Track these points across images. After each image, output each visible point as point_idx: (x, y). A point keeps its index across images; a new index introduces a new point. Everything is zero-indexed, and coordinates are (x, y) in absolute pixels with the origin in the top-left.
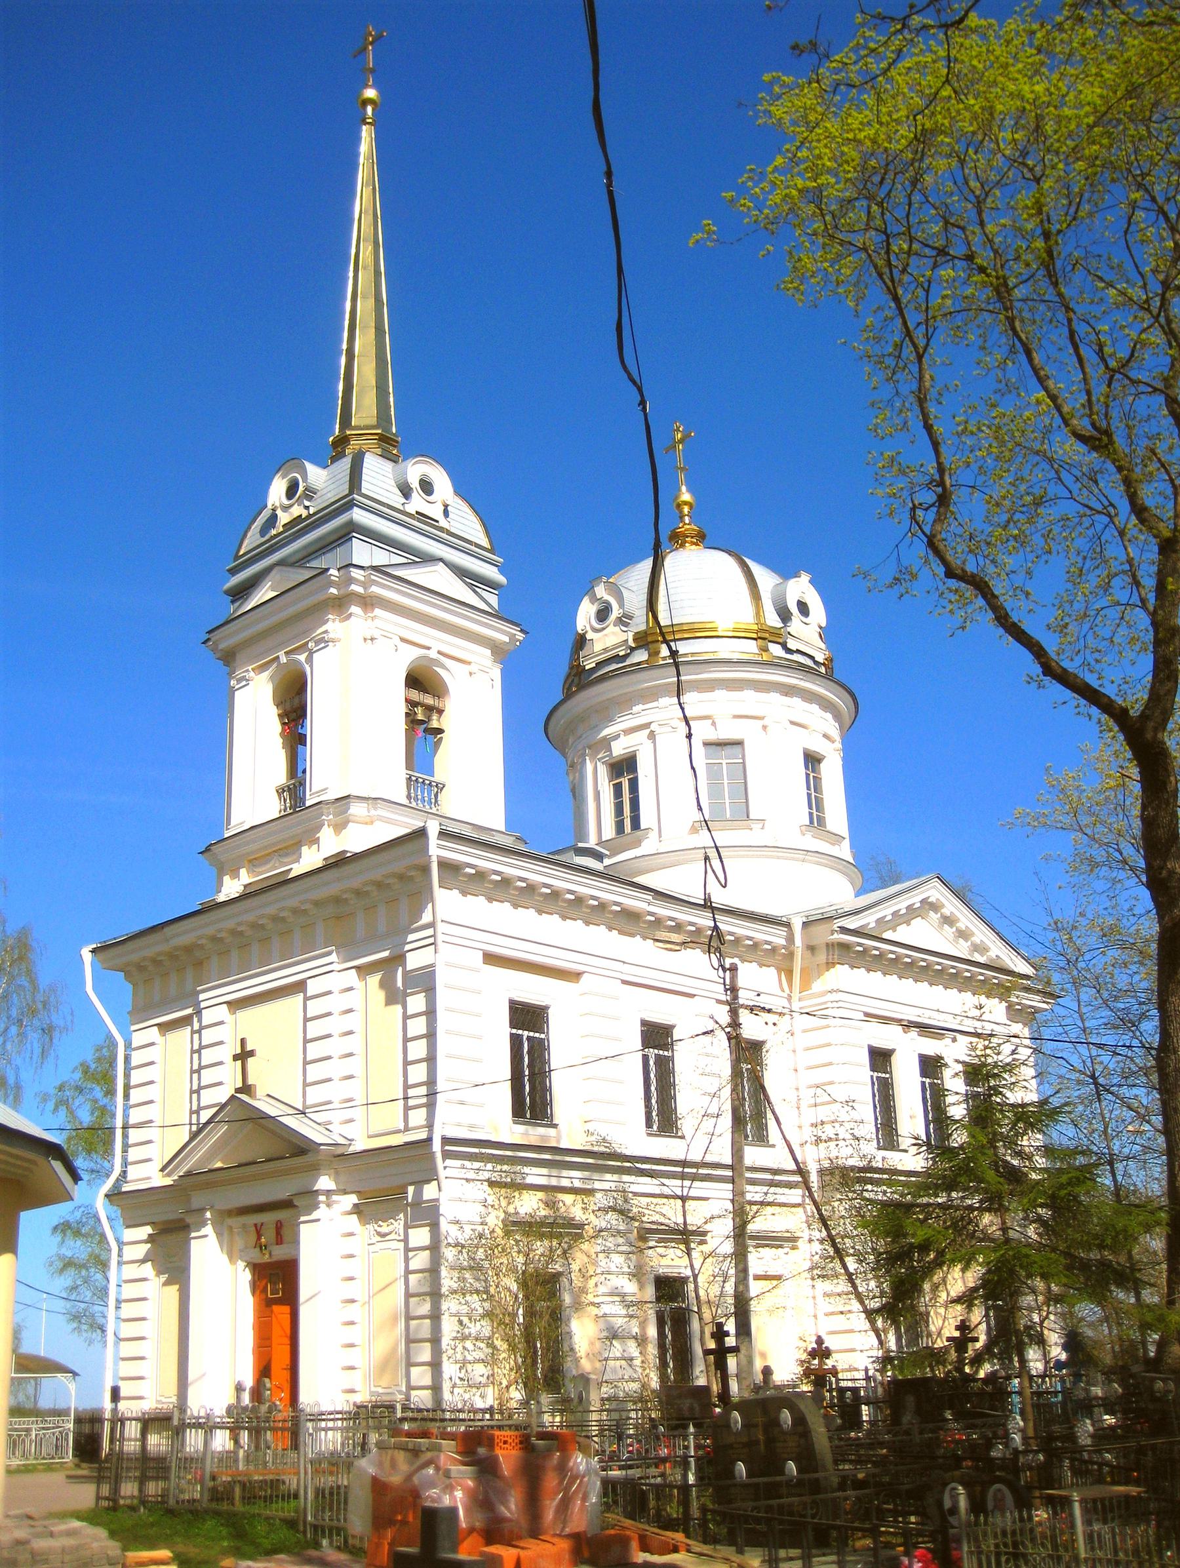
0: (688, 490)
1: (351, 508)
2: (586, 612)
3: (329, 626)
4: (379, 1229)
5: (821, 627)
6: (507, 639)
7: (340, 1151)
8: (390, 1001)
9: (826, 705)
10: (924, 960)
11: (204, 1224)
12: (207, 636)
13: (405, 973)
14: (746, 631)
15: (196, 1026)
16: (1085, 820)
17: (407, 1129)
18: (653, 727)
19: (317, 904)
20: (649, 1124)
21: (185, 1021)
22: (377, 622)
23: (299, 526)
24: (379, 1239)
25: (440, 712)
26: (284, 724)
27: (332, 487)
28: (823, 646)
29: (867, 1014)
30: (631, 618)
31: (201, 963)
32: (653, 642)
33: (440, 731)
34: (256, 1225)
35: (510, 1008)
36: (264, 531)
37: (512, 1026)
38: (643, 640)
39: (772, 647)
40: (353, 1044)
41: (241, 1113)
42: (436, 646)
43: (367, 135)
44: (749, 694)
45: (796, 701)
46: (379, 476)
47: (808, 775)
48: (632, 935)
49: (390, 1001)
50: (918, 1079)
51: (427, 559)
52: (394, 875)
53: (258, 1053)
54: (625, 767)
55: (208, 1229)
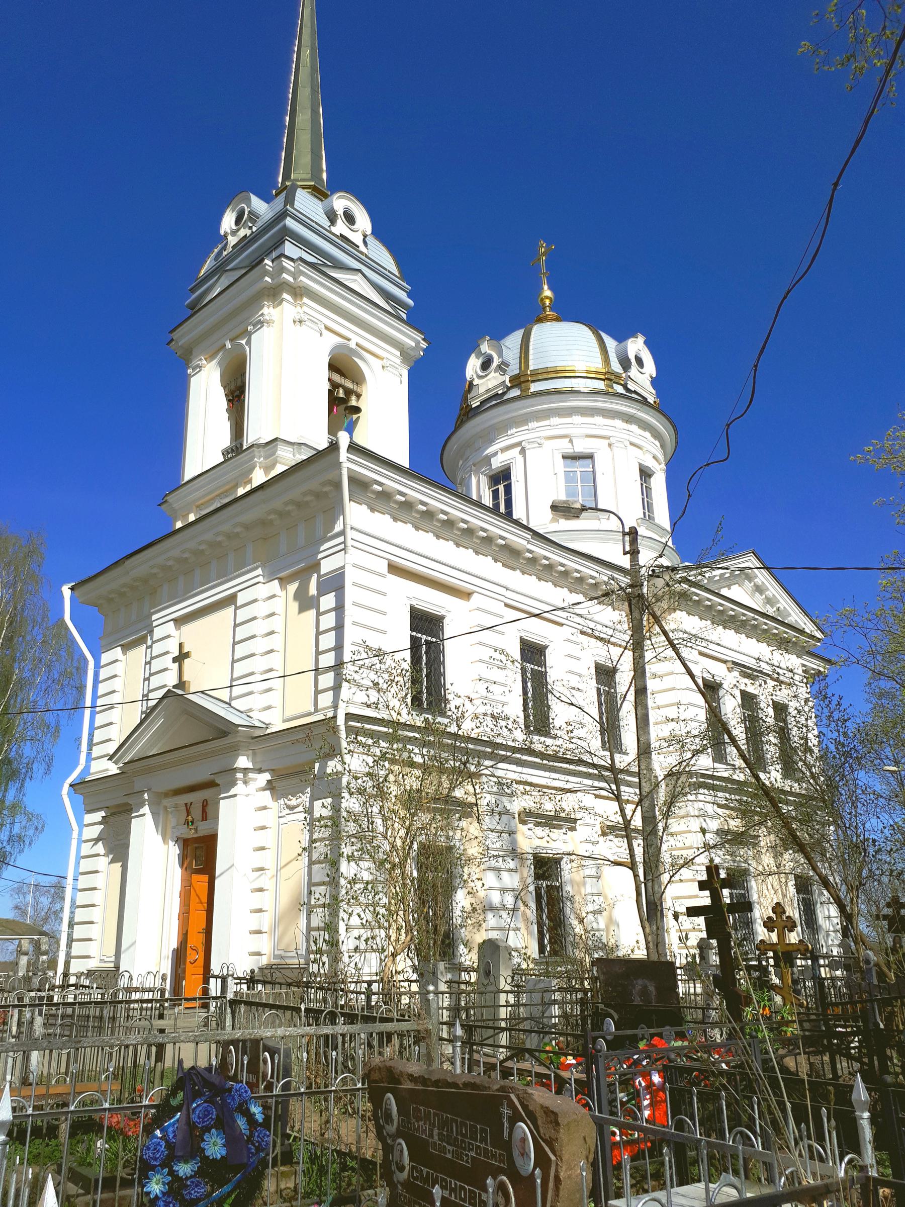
0: (550, 288)
1: (285, 218)
2: (473, 365)
3: (265, 310)
4: (289, 803)
6: (413, 344)
7: (258, 733)
8: (301, 610)
9: (656, 435)
11: (142, 805)
13: (319, 577)
14: (597, 373)
15: (149, 642)
17: (316, 710)
18: (523, 444)
19: (247, 527)
21: (141, 641)
22: (305, 308)
23: (245, 242)
24: (288, 811)
25: (359, 396)
26: (229, 401)
28: (654, 392)
30: (508, 365)
32: (524, 382)
33: (357, 410)
34: (186, 804)
36: (216, 258)
38: (519, 381)
39: (615, 385)
40: (275, 642)
41: (176, 703)
44: (599, 420)
45: (634, 428)
47: (642, 485)
48: (514, 569)
49: (301, 610)
52: (310, 492)
53: (193, 655)
54: (502, 478)
55: (146, 810)
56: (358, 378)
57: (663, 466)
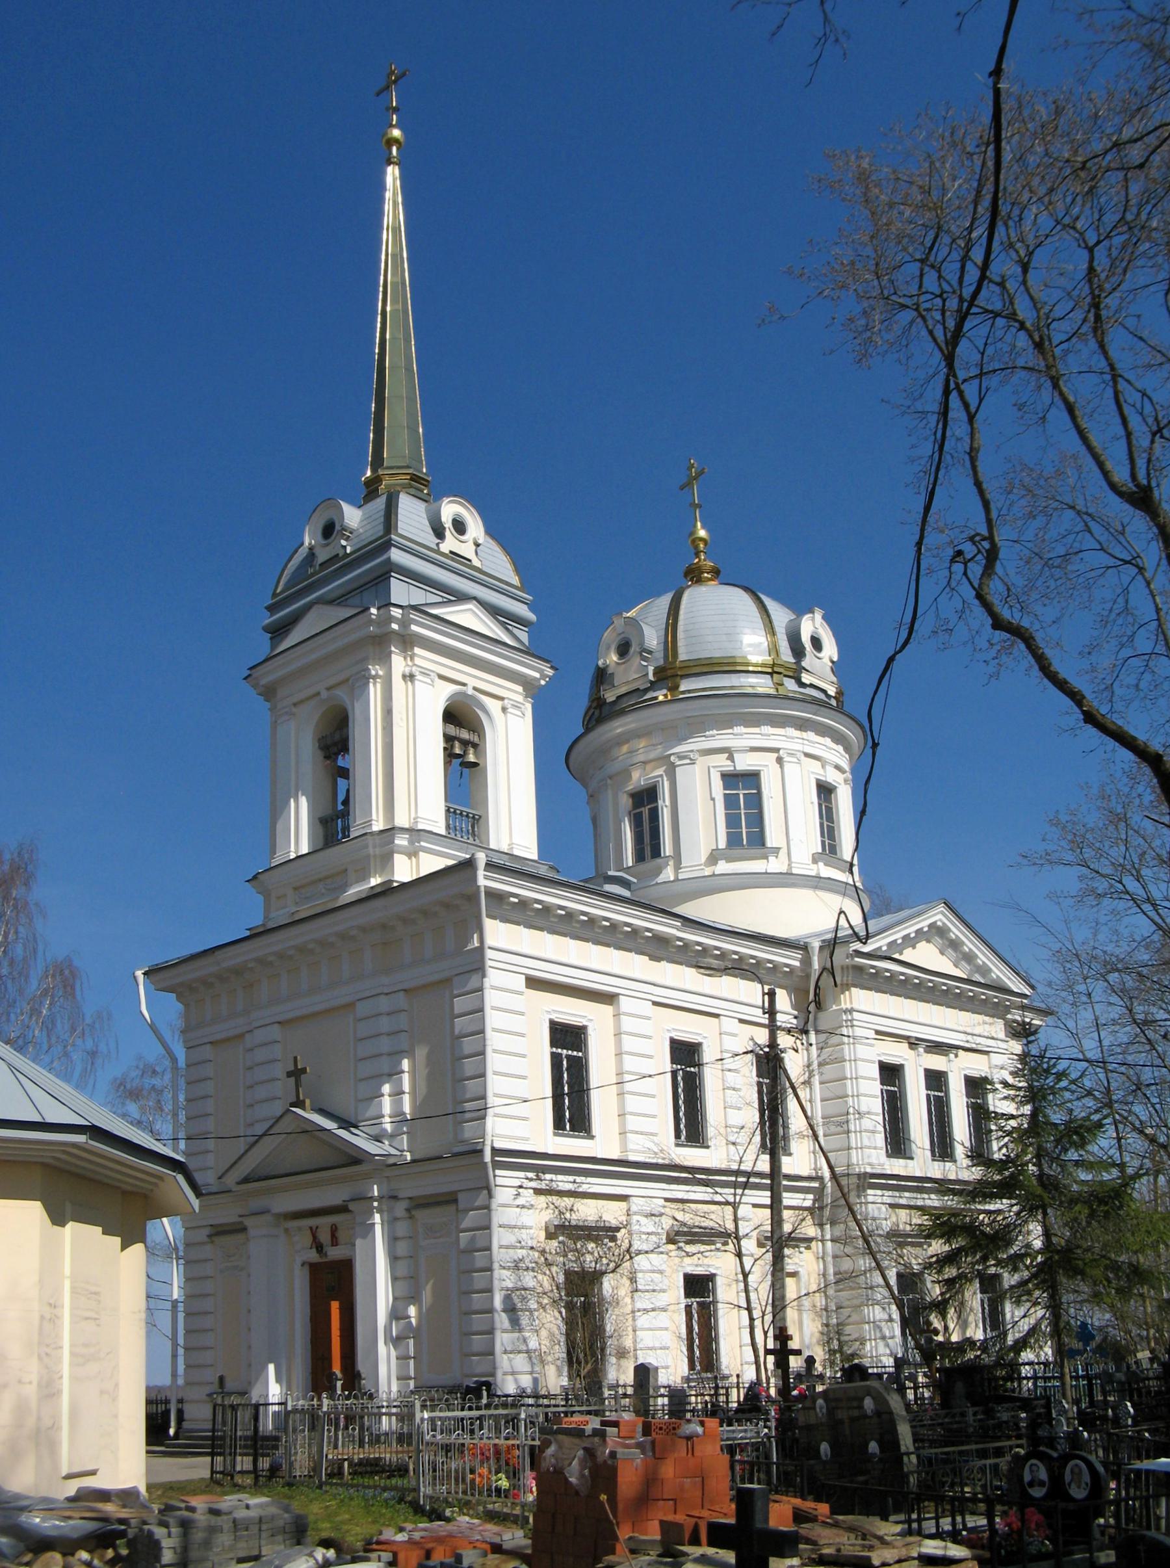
0: (703, 527)
5: (833, 662)
7: (391, 1161)
9: (838, 738)
10: (931, 981)
12: (249, 672)
16: (1088, 853)
19: (363, 929)
20: (678, 1135)
27: (368, 527)
28: (835, 679)
29: (878, 1032)
31: (251, 985)
35: (551, 1028)
37: (553, 1044)
42: (472, 683)
43: (392, 175)
45: (811, 735)
46: (411, 516)
50: (924, 1092)
51: (462, 597)
54: (647, 797)
56: (476, 728)
57: (849, 775)
